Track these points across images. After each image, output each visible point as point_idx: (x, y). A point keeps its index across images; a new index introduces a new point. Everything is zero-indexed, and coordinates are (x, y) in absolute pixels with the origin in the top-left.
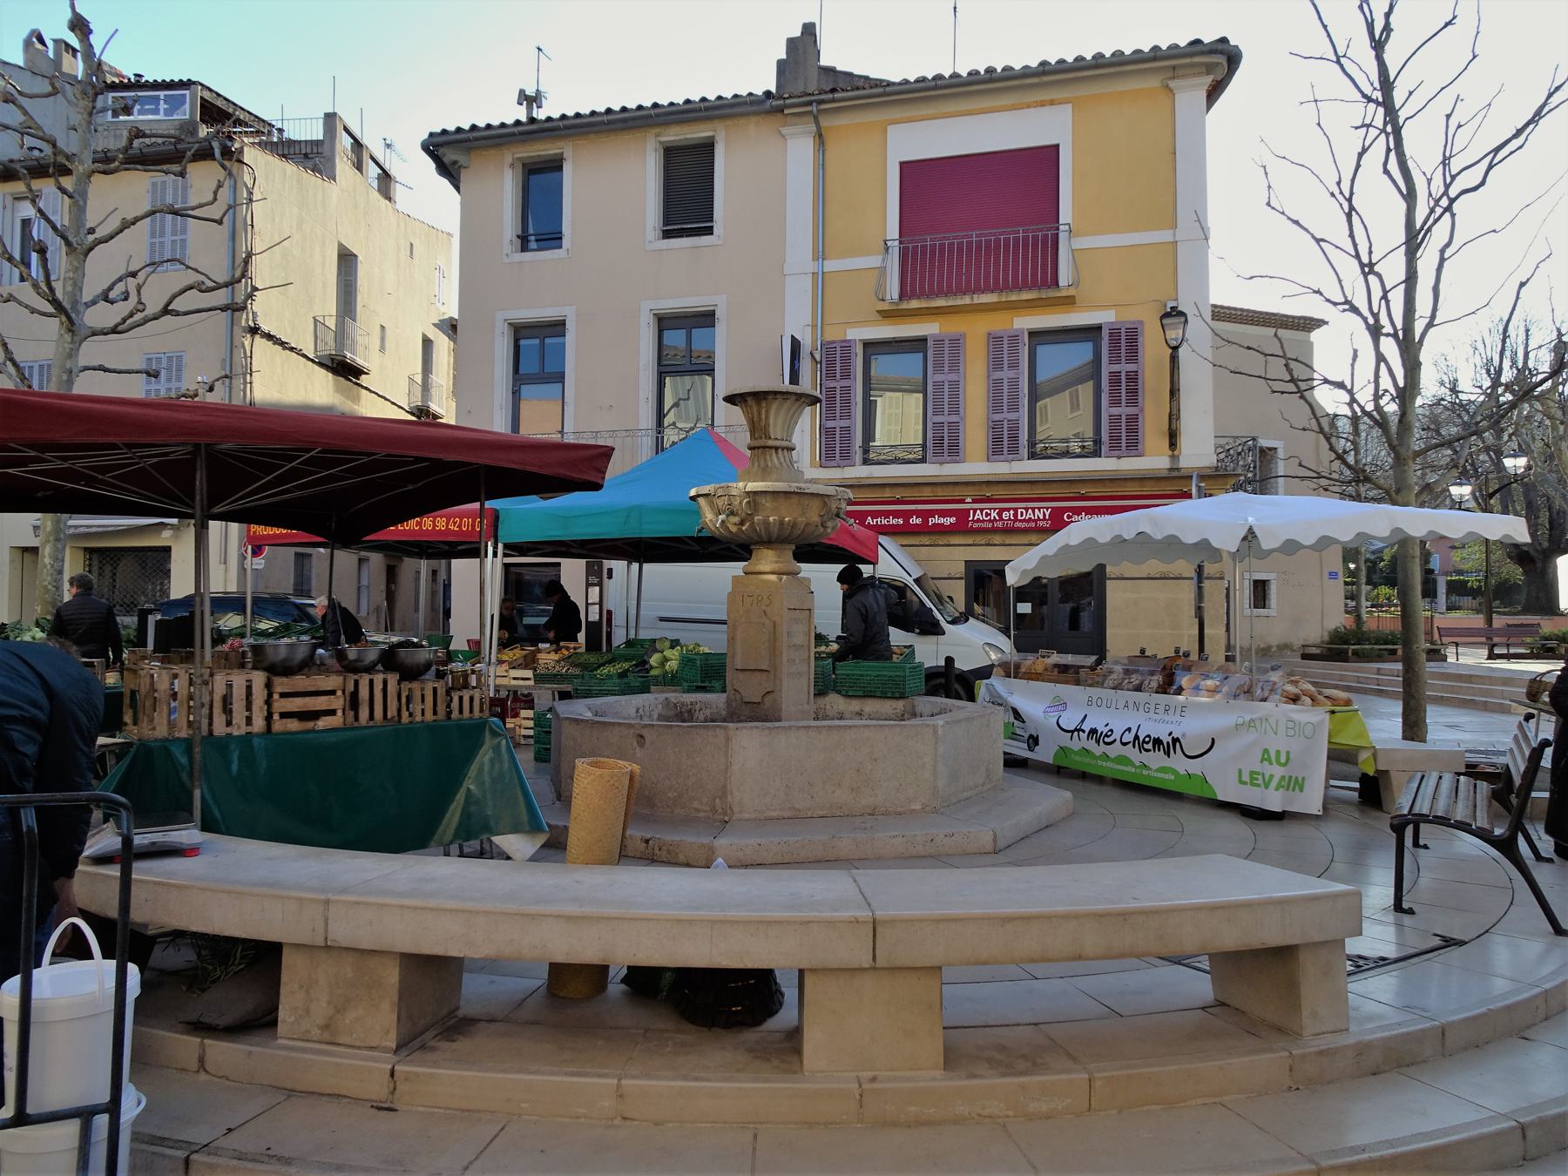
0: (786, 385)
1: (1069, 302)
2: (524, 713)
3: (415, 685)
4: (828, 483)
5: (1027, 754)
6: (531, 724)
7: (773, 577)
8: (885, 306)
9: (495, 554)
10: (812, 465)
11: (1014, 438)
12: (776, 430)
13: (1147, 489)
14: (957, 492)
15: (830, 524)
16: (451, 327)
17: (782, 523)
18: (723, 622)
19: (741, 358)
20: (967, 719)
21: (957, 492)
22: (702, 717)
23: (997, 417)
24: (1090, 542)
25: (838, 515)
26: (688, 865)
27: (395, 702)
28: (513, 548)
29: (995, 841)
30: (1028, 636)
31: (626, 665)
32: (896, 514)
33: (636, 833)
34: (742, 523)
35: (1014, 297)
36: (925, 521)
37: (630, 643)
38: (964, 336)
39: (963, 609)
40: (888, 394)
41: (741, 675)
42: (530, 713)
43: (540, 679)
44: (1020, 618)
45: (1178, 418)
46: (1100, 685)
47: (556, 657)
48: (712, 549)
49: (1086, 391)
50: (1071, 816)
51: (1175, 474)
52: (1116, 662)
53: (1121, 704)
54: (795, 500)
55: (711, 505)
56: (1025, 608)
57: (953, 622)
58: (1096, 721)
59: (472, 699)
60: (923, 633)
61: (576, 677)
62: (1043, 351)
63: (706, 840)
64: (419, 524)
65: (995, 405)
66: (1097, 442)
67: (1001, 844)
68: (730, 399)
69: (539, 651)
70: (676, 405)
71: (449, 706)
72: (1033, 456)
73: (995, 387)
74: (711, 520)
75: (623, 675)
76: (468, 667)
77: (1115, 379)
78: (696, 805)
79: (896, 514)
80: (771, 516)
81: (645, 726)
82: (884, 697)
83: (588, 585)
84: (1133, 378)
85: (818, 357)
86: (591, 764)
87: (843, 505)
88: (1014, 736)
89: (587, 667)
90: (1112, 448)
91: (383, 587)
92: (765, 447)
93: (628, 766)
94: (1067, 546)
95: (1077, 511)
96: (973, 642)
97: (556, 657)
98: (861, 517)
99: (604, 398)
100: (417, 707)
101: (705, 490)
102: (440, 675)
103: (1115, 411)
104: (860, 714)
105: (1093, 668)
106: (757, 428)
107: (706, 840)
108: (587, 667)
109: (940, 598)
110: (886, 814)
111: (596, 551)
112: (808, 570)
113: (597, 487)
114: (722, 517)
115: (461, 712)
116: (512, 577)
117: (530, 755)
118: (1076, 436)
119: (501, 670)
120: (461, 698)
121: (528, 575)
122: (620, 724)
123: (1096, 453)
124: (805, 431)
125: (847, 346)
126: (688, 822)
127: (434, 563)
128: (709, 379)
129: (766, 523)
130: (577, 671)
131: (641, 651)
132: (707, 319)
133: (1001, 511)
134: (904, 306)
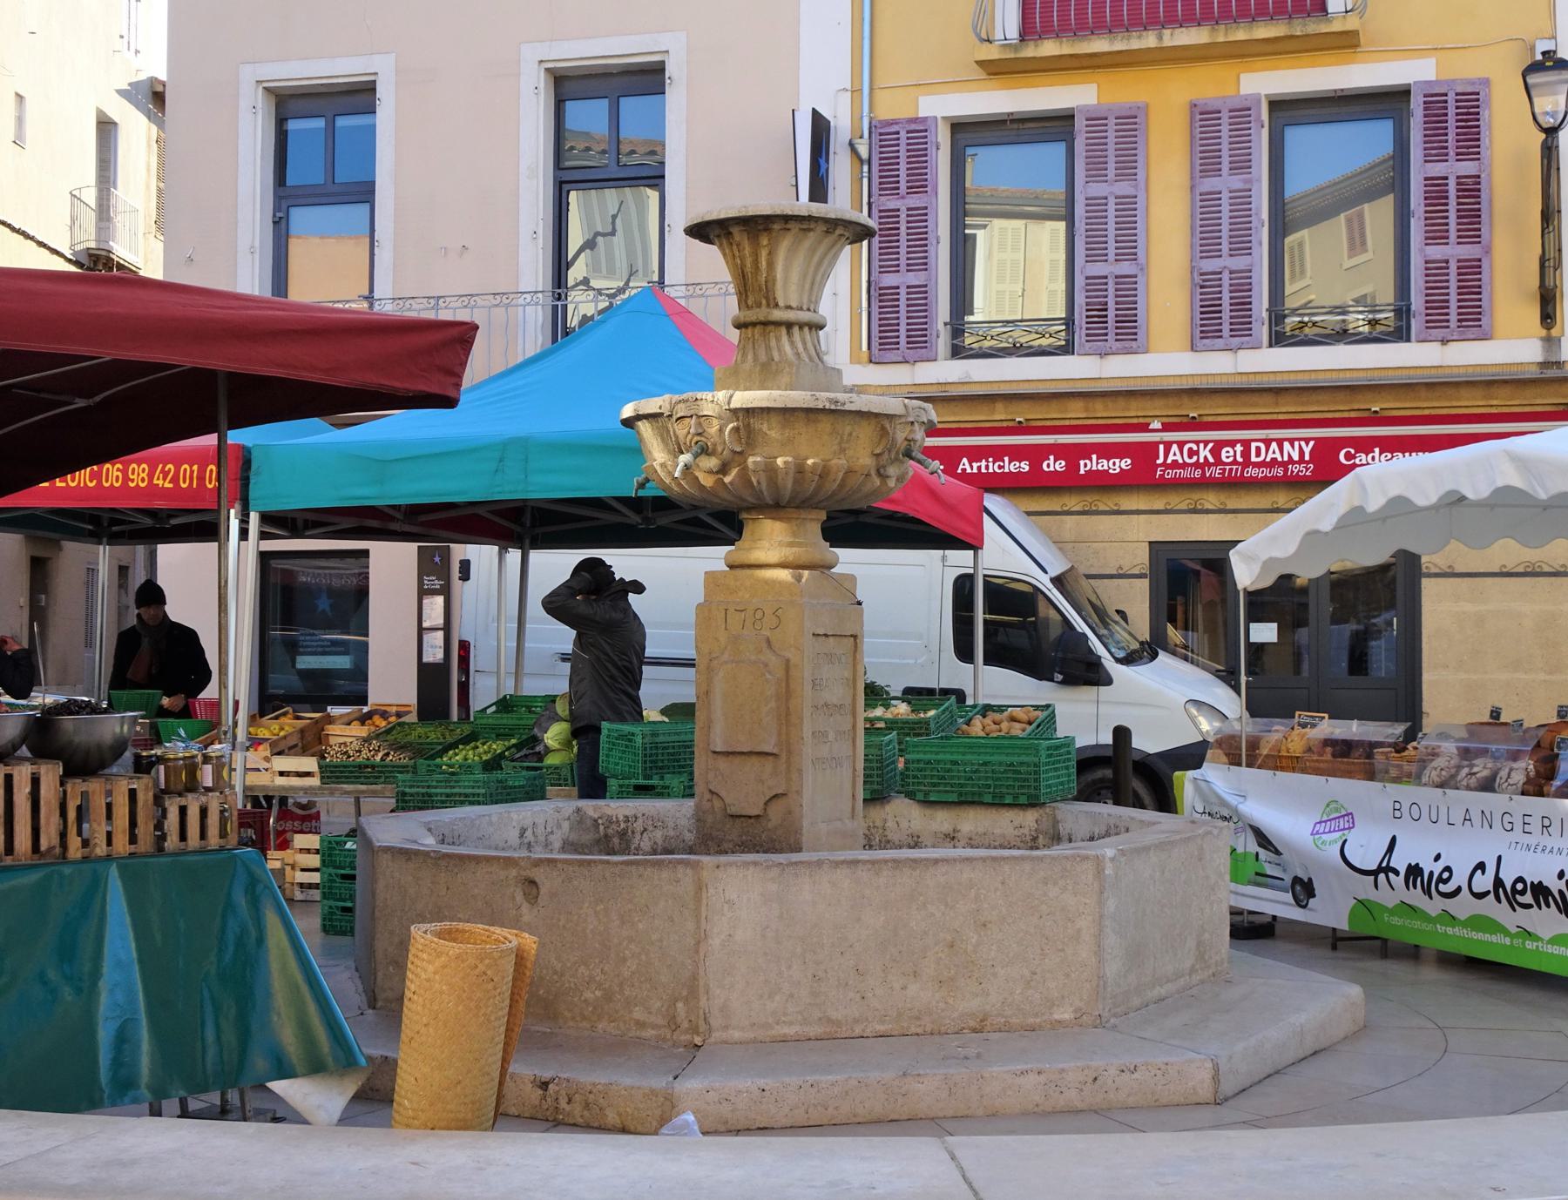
0: (803, 204)
1: (1346, 43)
2: (301, 841)
3: (94, 786)
4: (886, 390)
5: (1296, 914)
6: (315, 861)
7: (784, 575)
8: (992, 53)
9: (244, 534)
10: (855, 359)
11: (1243, 305)
12: (788, 289)
13: (1516, 403)
14: (1134, 411)
15: (892, 471)
16: (154, 98)
17: (800, 469)
18: (689, 663)
19: (717, 152)
20: (1160, 846)
21: (1134, 411)
22: (646, 845)
23: (1209, 265)
24: (1399, 506)
25: (908, 454)
26: (624, 1130)
27: (56, 818)
28: (277, 522)
29: (1216, 1078)
30: (1272, 688)
31: (498, 747)
32: (1016, 453)
33: (524, 1069)
34: (724, 469)
35: (1240, 34)
36: (1073, 466)
37: (505, 705)
38: (1145, 109)
39: (1145, 635)
40: (998, 223)
41: (722, 764)
42: (313, 841)
43: (332, 774)
44: (1257, 650)
45: (1558, 265)
46: (1415, 778)
47: (363, 731)
48: (664, 520)
49: (1379, 216)
50: (1362, 1031)
51: (1551, 373)
52: (1443, 736)
53: (1457, 817)
54: (825, 425)
55: (664, 434)
56: (1265, 633)
57: (1129, 660)
58: (1414, 850)
59: (204, 812)
60: (1071, 681)
61: (403, 769)
62: (1297, 138)
63: (659, 1082)
64: (95, 476)
65: (1205, 239)
66: (1403, 312)
67: (1228, 1087)
68: (701, 231)
69: (330, 720)
70: (590, 245)
71: (159, 826)
72: (1279, 339)
73: (1205, 211)
74: (665, 465)
75: (493, 765)
76: (194, 749)
77: (1436, 191)
78: (638, 1013)
79: (1016, 453)
80: (780, 455)
81: (538, 863)
82: (998, 804)
83: (423, 593)
84: (1471, 189)
85: (863, 151)
86: (440, 935)
87: (919, 434)
88: (1261, 879)
89: (421, 751)
90: (1431, 324)
91: (24, 600)
92: (766, 322)
93: (511, 938)
94: (1358, 511)
95: (1365, 445)
96: (1165, 700)
97: (363, 731)
98: (950, 458)
99: (453, 226)
100: (97, 829)
101: (651, 405)
102: (143, 766)
103: (1436, 252)
104: (951, 838)
105: (1399, 748)
106: (752, 287)
107: (659, 1082)
108: (427, 752)
109: (1101, 613)
110: (1007, 1028)
111: (437, 525)
112: (858, 563)
113: (448, 402)
114: (685, 458)
115: (183, 836)
116: (275, 579)
117: (316, 922)
118: (1357, 301)
119: (255, 758)
120: (183, 811)
121: (306, 575)
122: (488, 859)
123: (1400, 334)
124: (841, 292)
125: (919, 129)
126: (619, 1047)
127: (122, 551)
128: (653, 195)
129: (770, 469)
130: (403, 759)
131: (529, 720)
132: (647, 78)
133: (1218, 446)
134: (1030, 51)
